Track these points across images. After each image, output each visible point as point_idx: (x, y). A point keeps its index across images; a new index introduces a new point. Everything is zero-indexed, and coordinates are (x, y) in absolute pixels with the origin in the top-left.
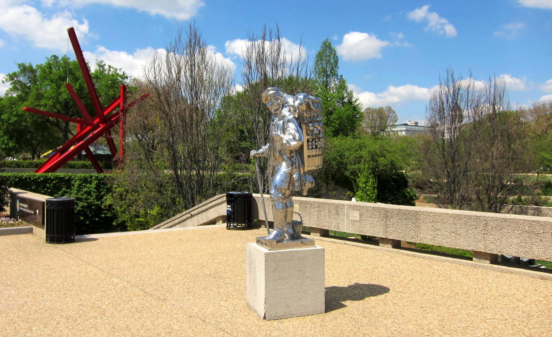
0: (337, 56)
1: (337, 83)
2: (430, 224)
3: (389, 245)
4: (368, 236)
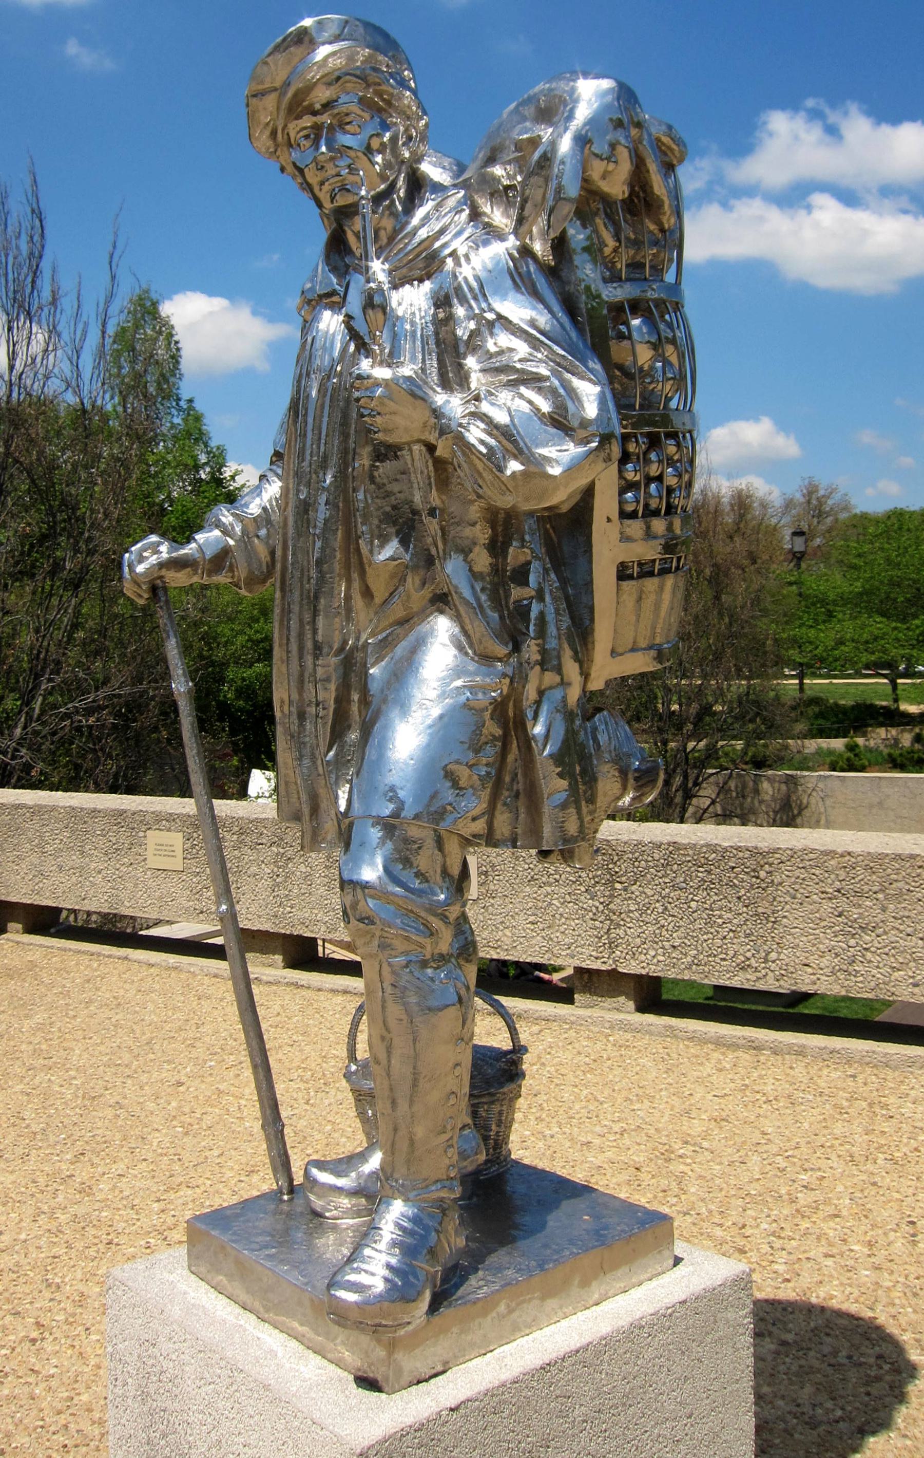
0: (177, 342)
1: (177, 420)
2: (827, 906)
3: (622, 999)
4: (517, 963)
